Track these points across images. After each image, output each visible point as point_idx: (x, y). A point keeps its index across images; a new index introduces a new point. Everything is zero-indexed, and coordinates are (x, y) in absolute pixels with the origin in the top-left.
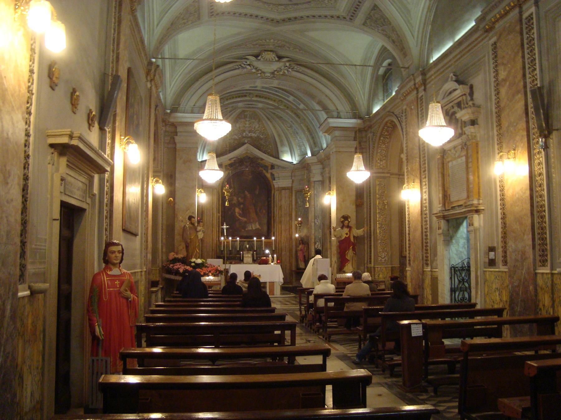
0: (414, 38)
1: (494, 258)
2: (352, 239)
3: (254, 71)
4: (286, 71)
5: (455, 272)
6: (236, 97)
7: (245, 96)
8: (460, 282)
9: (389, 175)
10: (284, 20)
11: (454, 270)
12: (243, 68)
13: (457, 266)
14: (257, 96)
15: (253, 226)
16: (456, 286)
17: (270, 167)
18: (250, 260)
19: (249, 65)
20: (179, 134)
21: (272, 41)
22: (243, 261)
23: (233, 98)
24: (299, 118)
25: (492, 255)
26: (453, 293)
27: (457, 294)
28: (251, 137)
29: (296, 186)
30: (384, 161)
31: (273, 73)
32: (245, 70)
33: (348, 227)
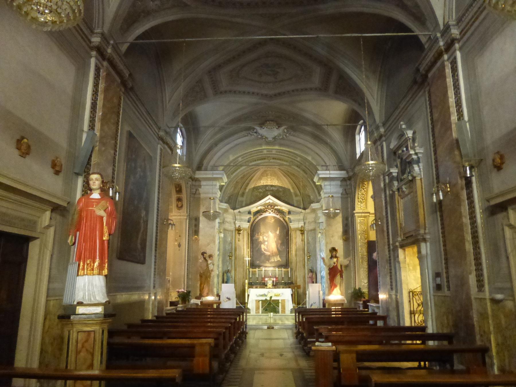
0: (374, 99)
1: (440, 283)
2: (339, 267)
3: (260, 137)
4: (284, 136)
5: (413, 296)
6: (258, 160)
7: (264, 159)
8: (419, 305)
9: (368, 214)
10: (275, 95)
11: (413, 294)
12: (251, 135)
13: (415, 290)
14: (273, 159)
15: (275, 258)
16: (415, 309)
17: (287, 213)
18: (271, 286)
19: (256, 132)
20: (202, 187)
21: (274, 113)
22: (266, 286)
23: (255, 161)
24: (307, 174)
25: (438, 280)
26: (413, 315)
27: (417, 316)
28: (272, 190)
29: (308, 227)
30: (364, 203)
31: (274, 138)
32: (253, 136)
33: (336, 257)
